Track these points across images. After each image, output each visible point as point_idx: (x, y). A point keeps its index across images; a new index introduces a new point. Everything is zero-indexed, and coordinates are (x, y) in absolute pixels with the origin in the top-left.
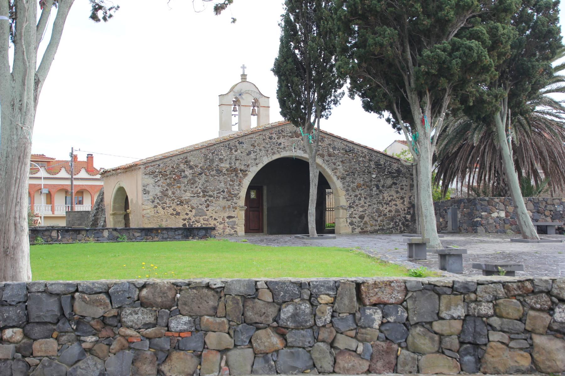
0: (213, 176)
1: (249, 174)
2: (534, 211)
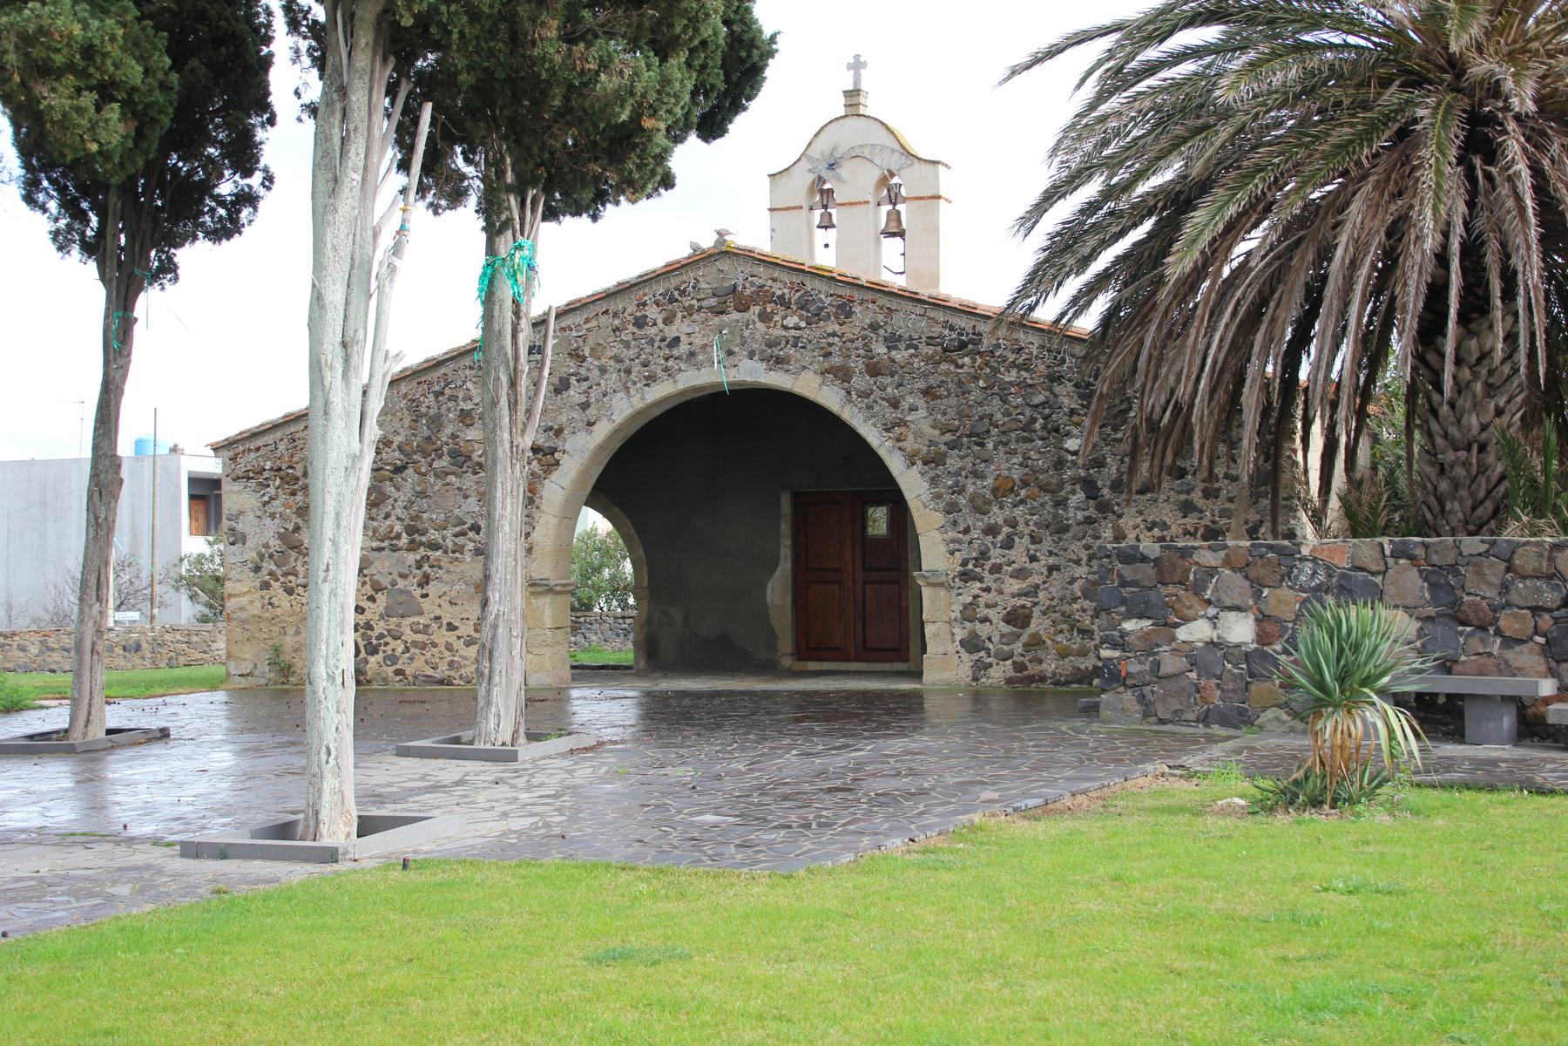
1: (565, 460)
2: (1431, 611)
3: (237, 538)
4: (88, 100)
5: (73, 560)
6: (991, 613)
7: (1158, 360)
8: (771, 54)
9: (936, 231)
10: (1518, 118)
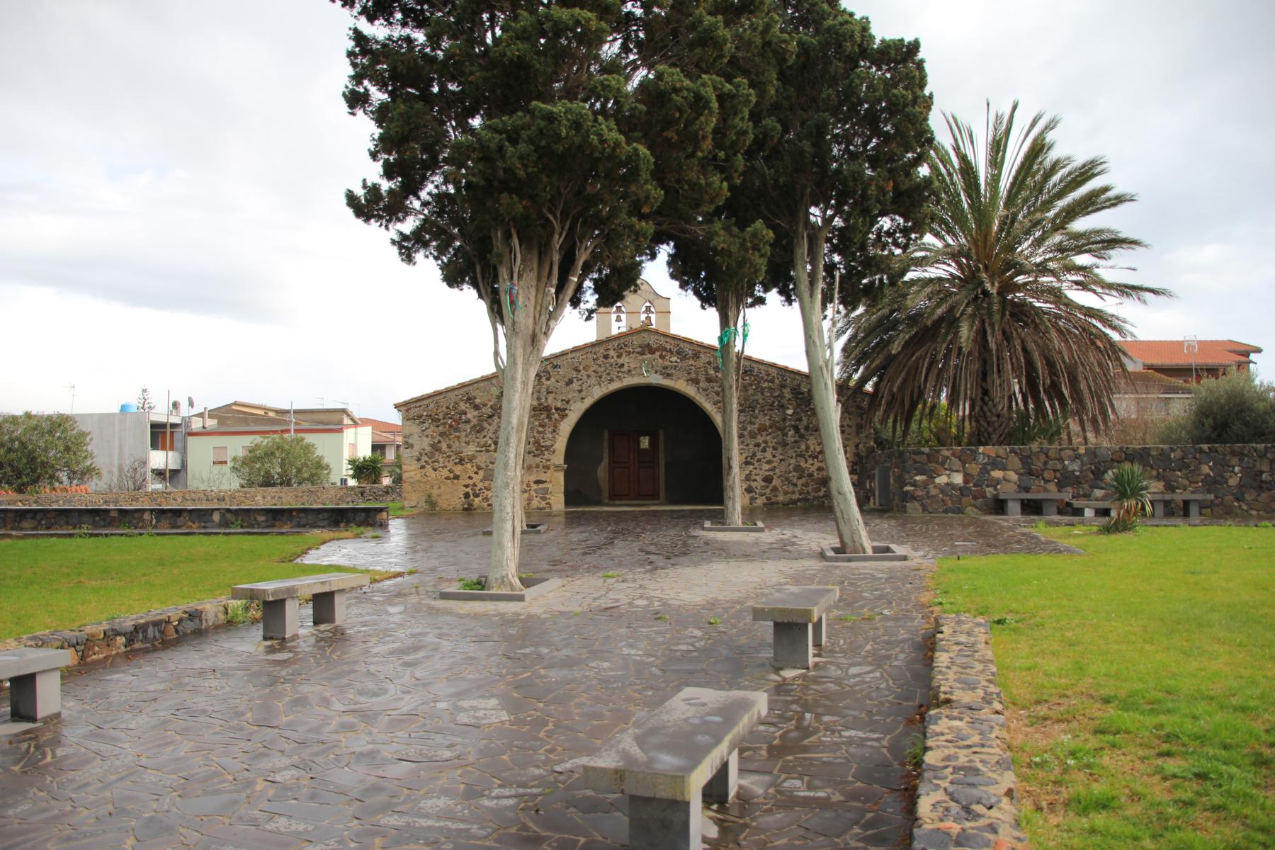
1: (570, 413)
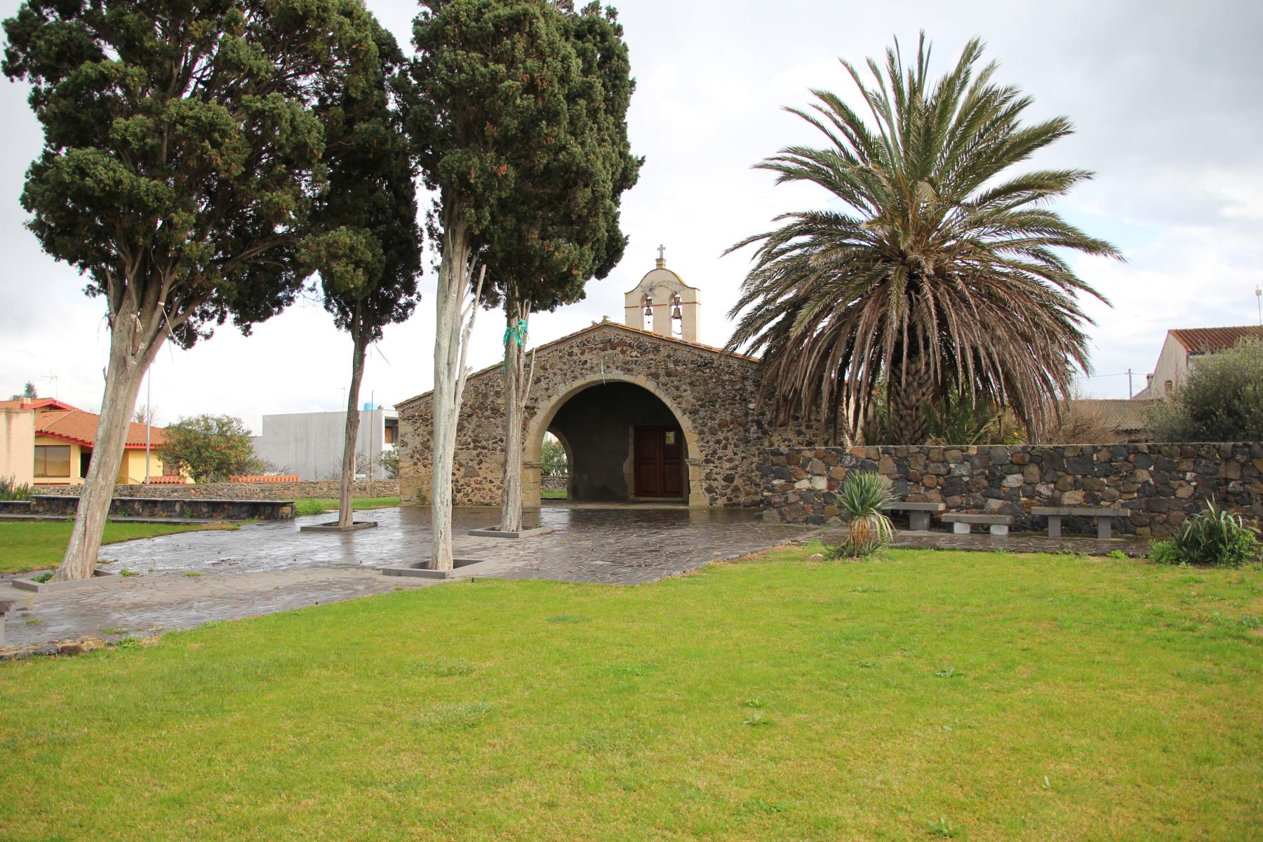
0: (487, 418)
1: (538, 412)
2: (897, 476)
3: (404, 444)
4: (351, 267)
5: (340, 453)
6: (718, 477)
7: (787, 371)
8: (626, 244)
9: (694, 316)
10: (927, 276)
